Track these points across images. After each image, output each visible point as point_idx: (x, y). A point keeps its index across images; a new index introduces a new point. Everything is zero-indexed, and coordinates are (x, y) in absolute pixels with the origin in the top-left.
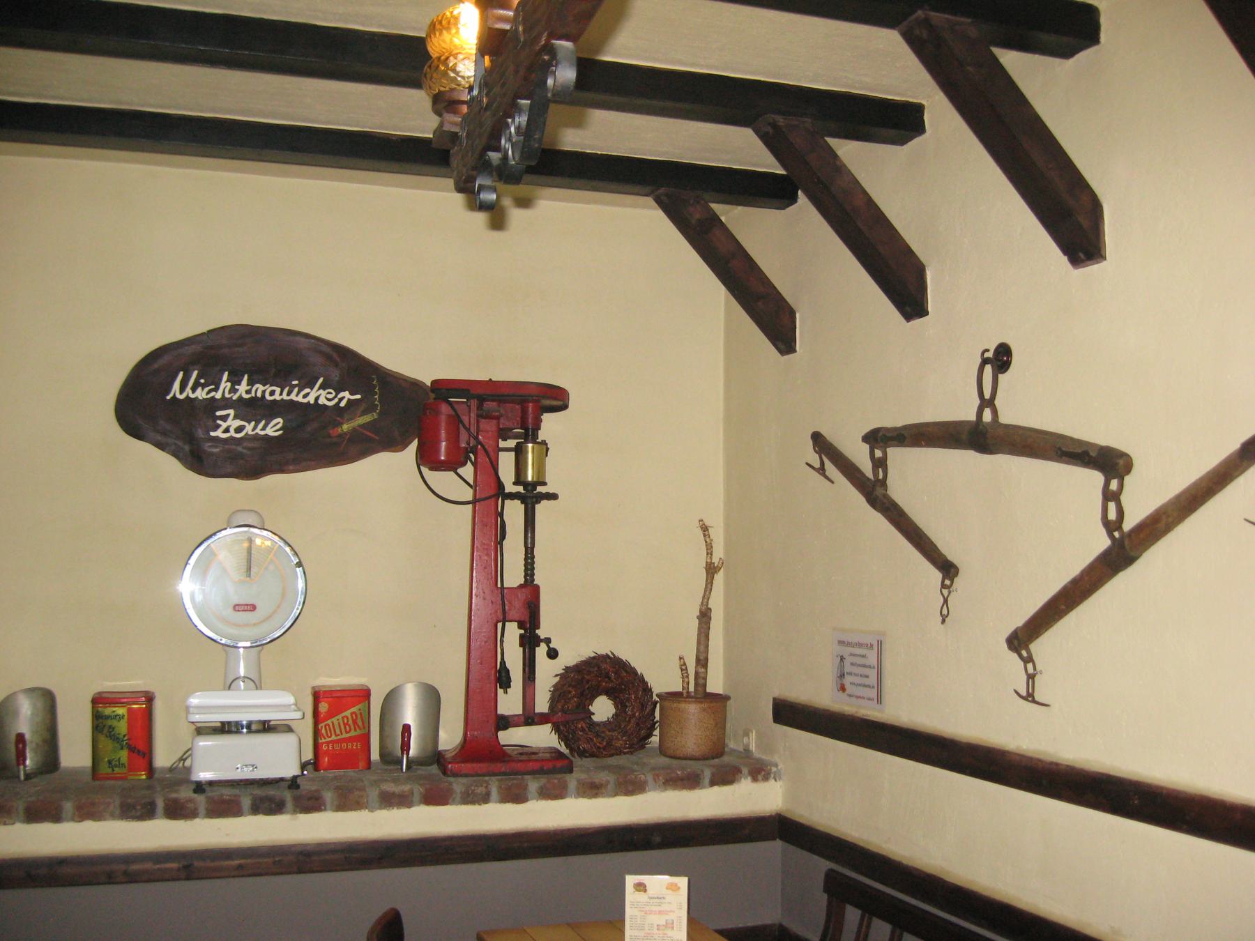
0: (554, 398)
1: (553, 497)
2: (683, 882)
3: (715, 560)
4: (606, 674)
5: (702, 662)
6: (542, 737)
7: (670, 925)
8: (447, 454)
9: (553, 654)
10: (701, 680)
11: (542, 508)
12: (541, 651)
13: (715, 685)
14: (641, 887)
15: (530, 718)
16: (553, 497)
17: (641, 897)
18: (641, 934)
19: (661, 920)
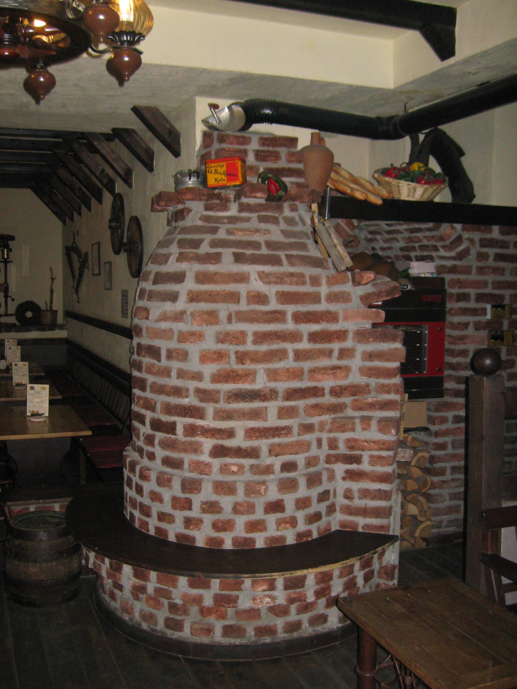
0: (12, 238)
1: (11, 262)
2: (47, 387)
3: (54, 277)
4: (30, 305)
5: (51, 302)
6: (12, 320)
7: (42, 402)
8: (490, 572)
9: (13, 300)
10: (51, 307)
11: (8, 265)
12: (9, 299)
13: (54, 308)
14: (32, 388)
15: (6, 315)
16: (11, 262)
17: (32, 392)
18: (33, 405)
19: (39, 400)
